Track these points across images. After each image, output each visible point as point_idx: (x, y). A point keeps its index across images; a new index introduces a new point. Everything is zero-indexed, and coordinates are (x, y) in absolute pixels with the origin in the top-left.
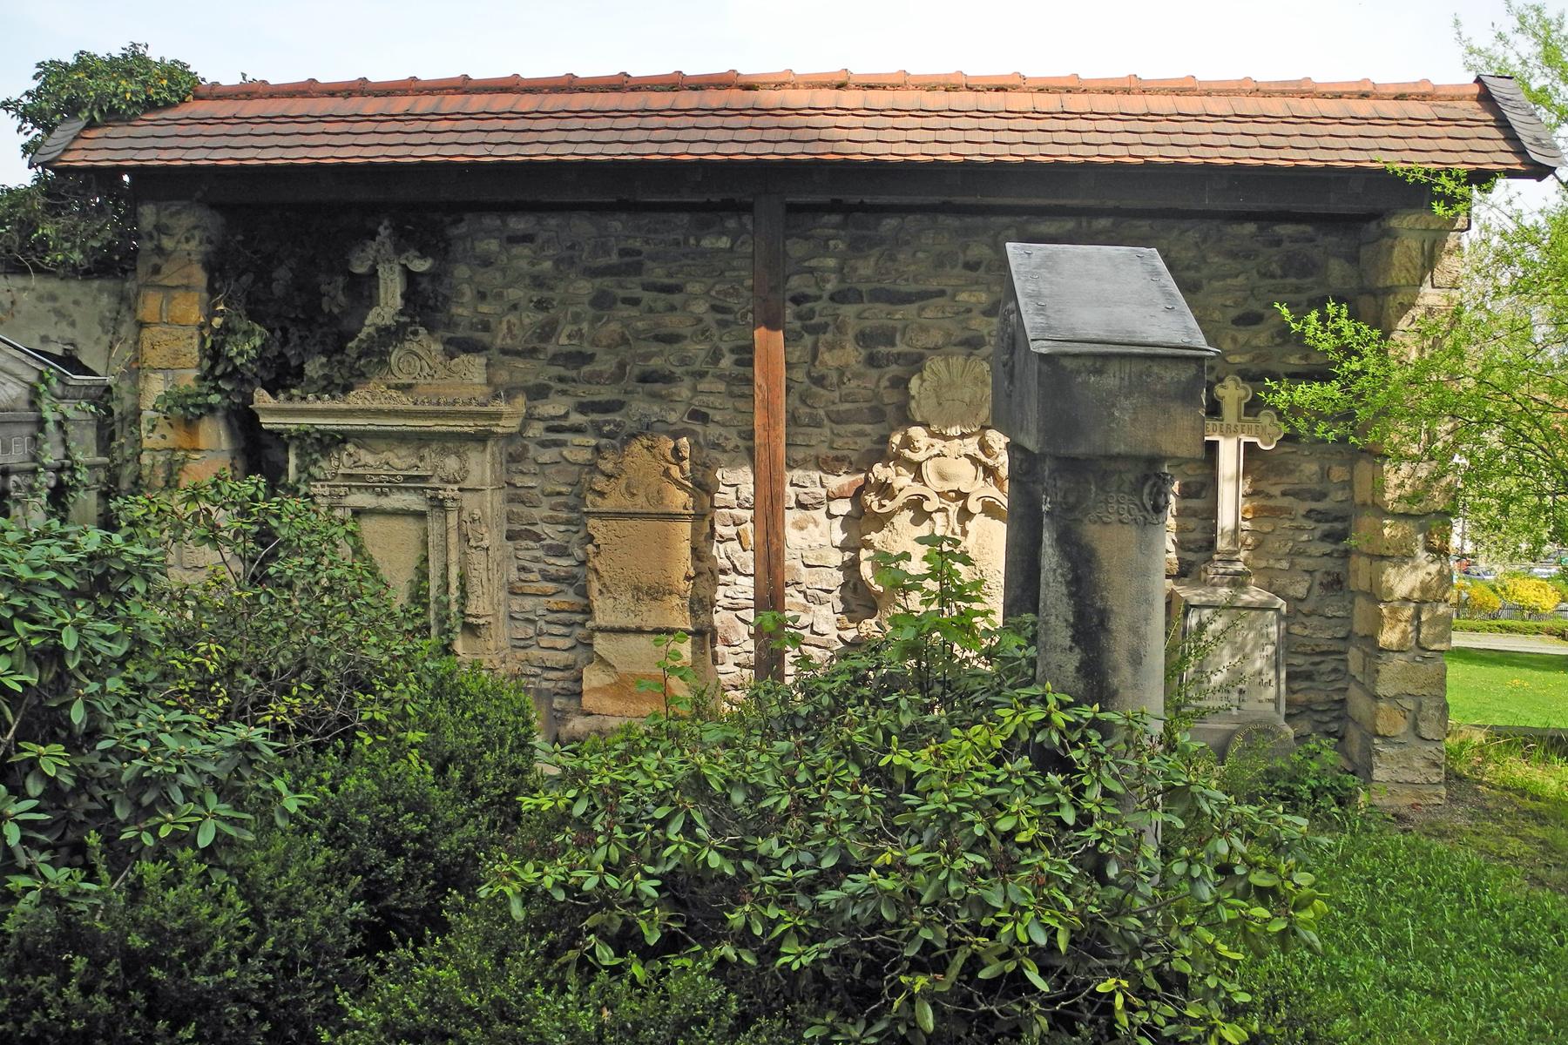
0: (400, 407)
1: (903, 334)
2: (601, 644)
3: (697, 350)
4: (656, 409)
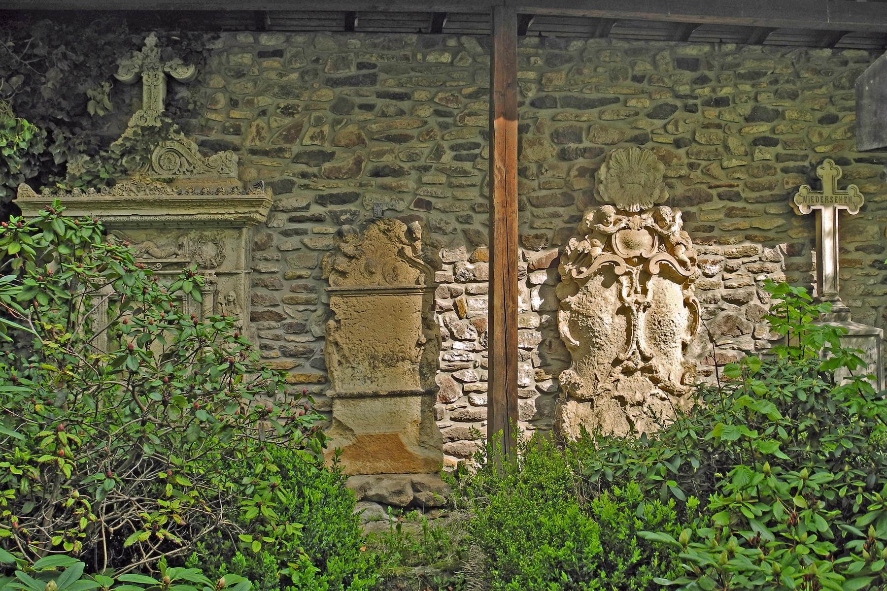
0: (164, 197)
1: (588, 133)
2: (339, 410)
3: (423, 148)
4: (387, 199)
